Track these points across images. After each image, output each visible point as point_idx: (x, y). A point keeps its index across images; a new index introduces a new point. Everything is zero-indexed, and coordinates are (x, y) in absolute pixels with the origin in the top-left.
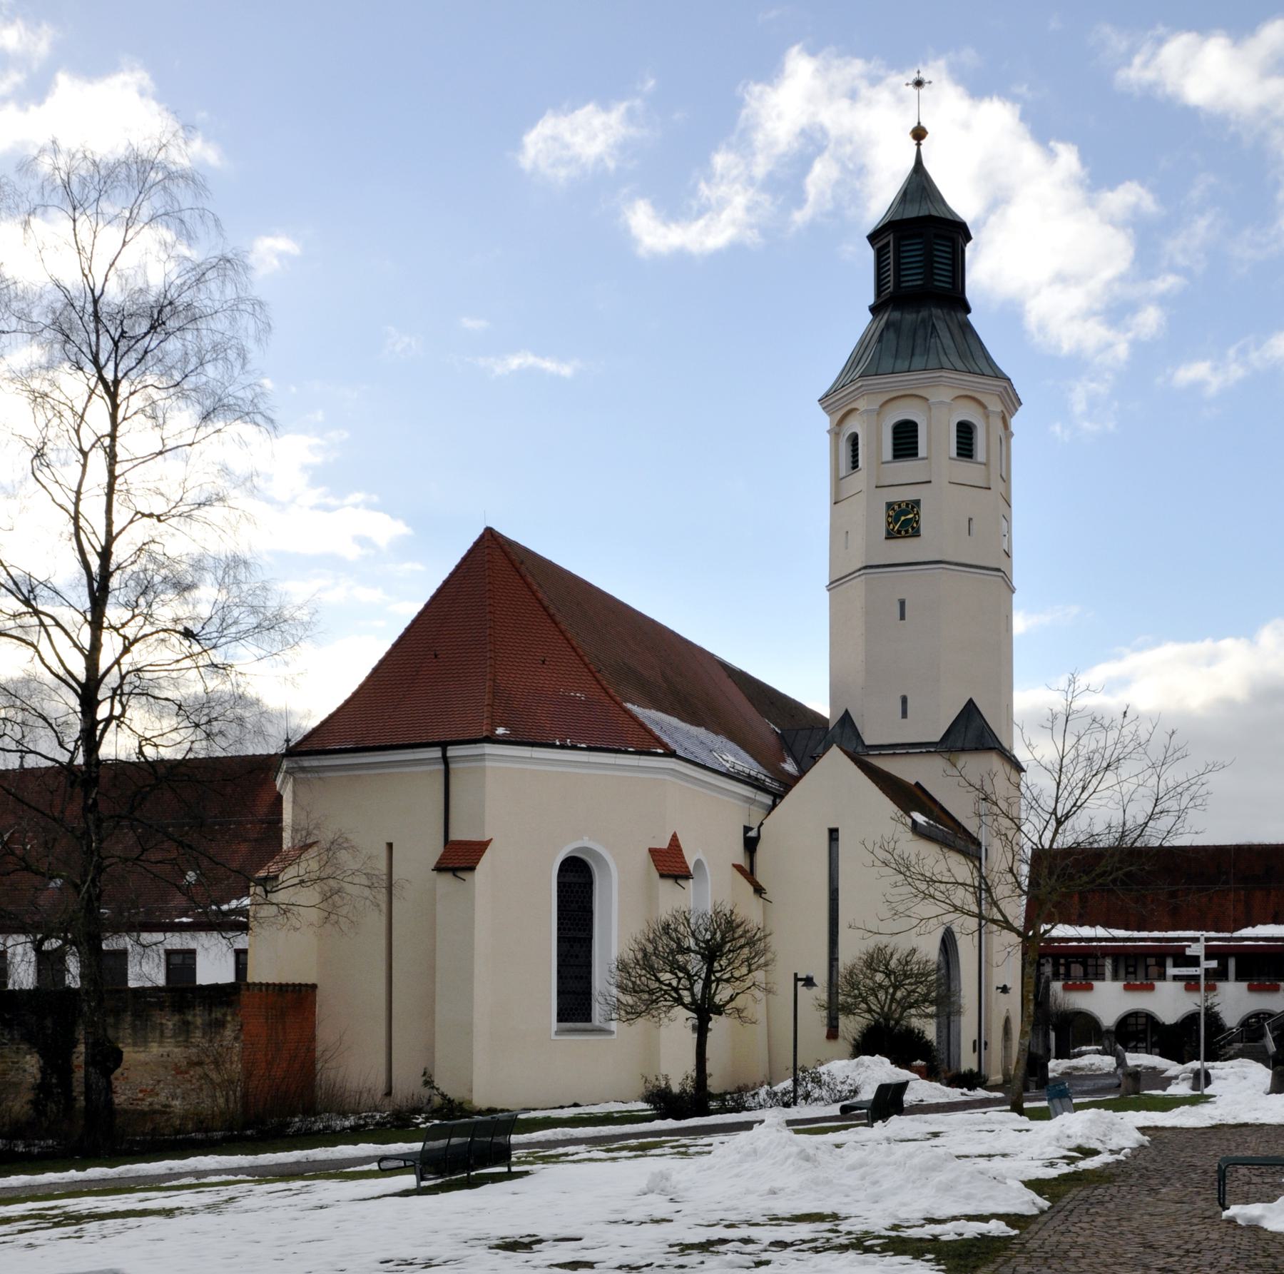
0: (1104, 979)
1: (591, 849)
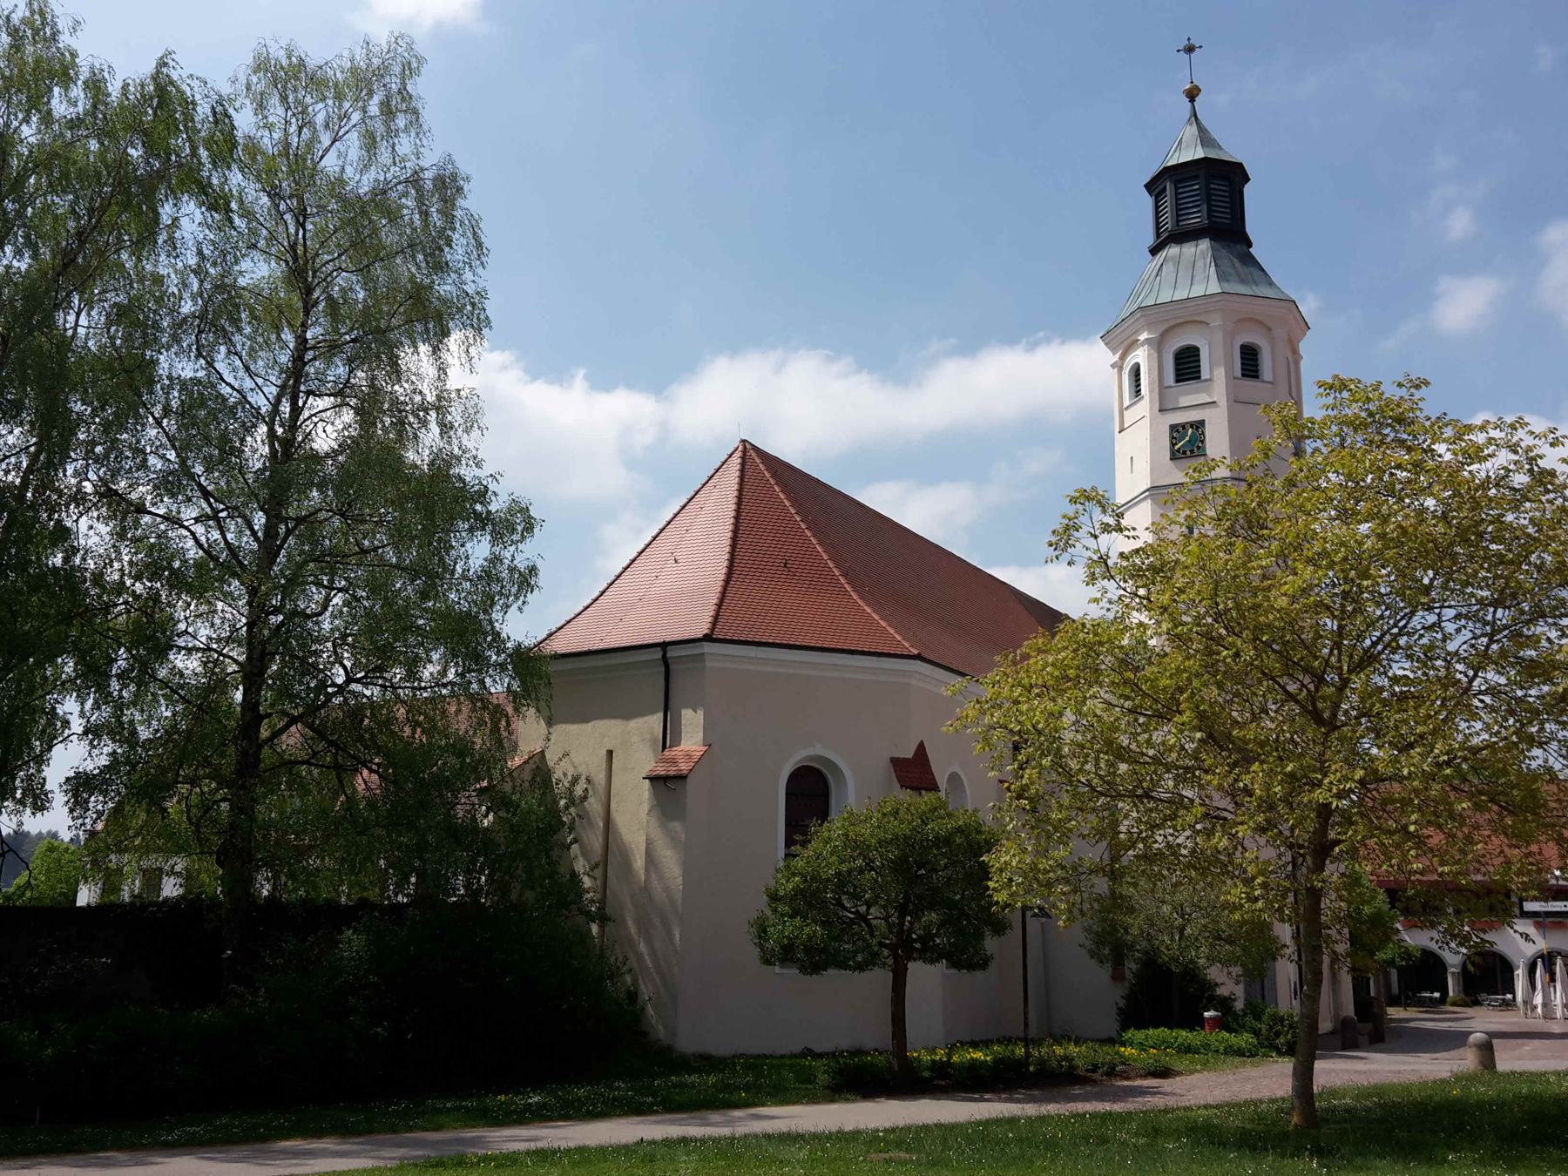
1: (834, 764)
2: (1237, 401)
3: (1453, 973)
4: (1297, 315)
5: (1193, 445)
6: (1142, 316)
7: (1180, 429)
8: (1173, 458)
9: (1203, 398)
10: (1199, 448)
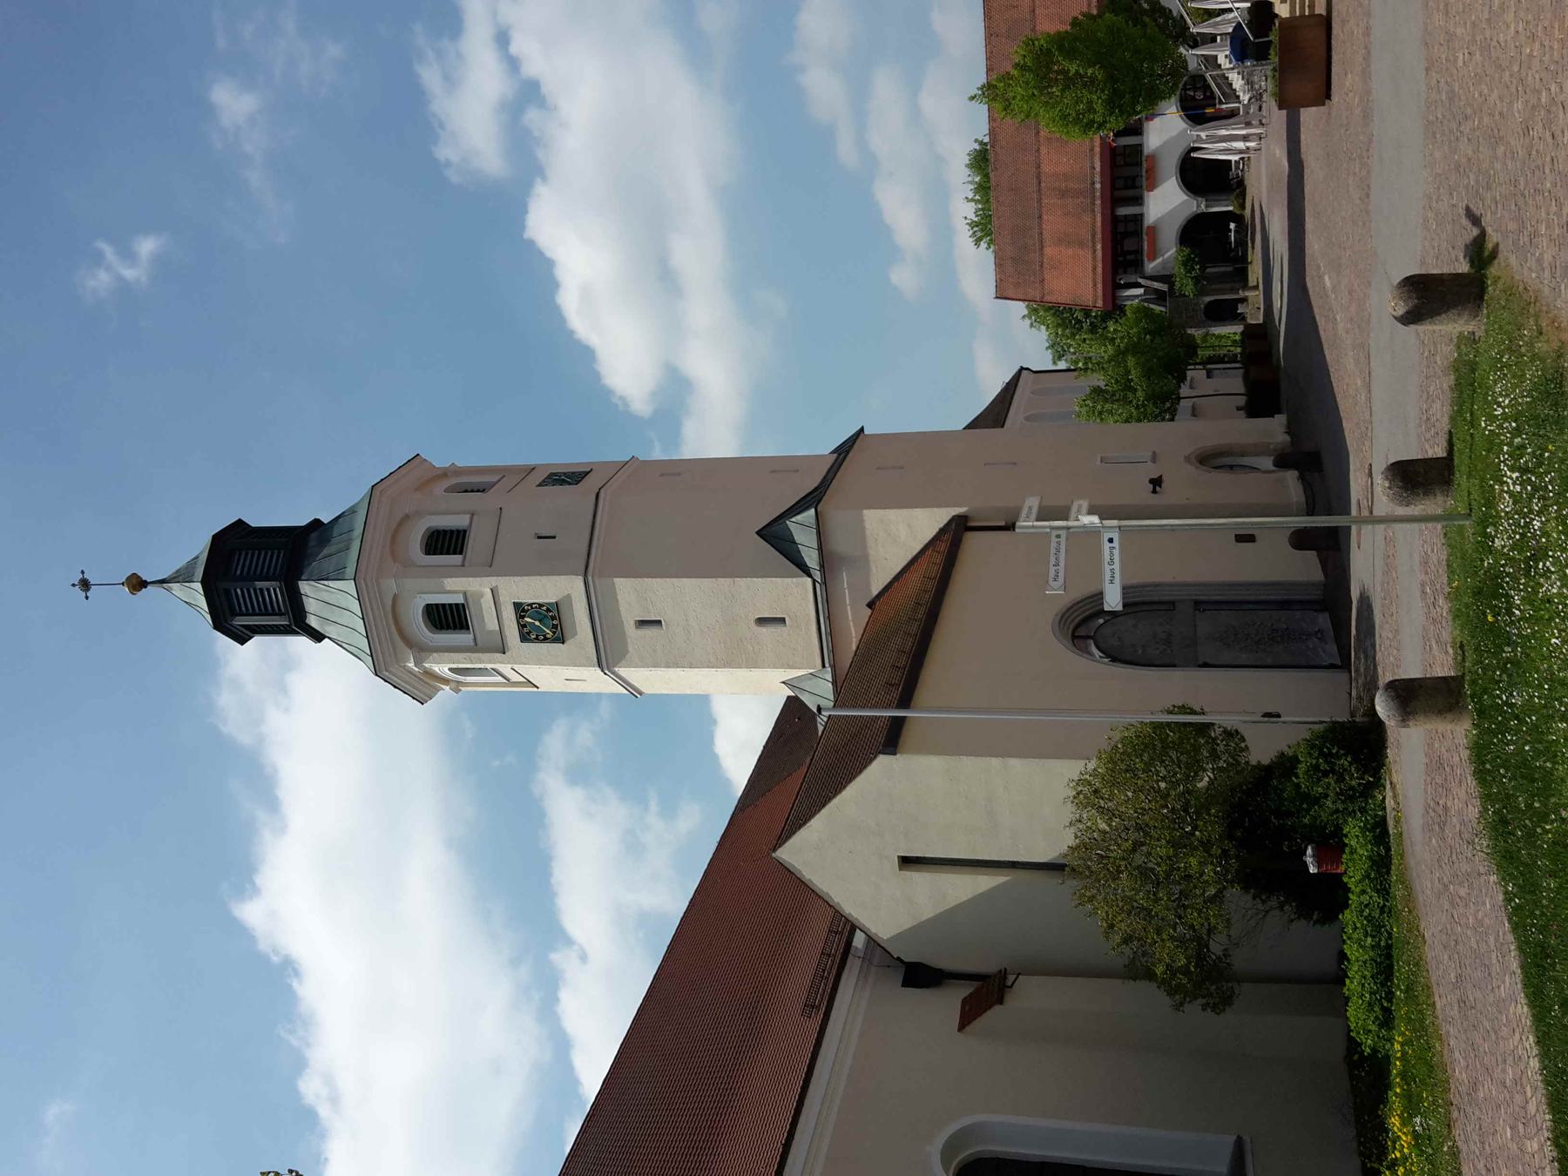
0: (1142, 215)
2: (490, 566)
3: (1207, 206)
4: (402, 471)
5: (546, 616)
6: (387, 671)
8: (561, 640)
10: (548, 610)
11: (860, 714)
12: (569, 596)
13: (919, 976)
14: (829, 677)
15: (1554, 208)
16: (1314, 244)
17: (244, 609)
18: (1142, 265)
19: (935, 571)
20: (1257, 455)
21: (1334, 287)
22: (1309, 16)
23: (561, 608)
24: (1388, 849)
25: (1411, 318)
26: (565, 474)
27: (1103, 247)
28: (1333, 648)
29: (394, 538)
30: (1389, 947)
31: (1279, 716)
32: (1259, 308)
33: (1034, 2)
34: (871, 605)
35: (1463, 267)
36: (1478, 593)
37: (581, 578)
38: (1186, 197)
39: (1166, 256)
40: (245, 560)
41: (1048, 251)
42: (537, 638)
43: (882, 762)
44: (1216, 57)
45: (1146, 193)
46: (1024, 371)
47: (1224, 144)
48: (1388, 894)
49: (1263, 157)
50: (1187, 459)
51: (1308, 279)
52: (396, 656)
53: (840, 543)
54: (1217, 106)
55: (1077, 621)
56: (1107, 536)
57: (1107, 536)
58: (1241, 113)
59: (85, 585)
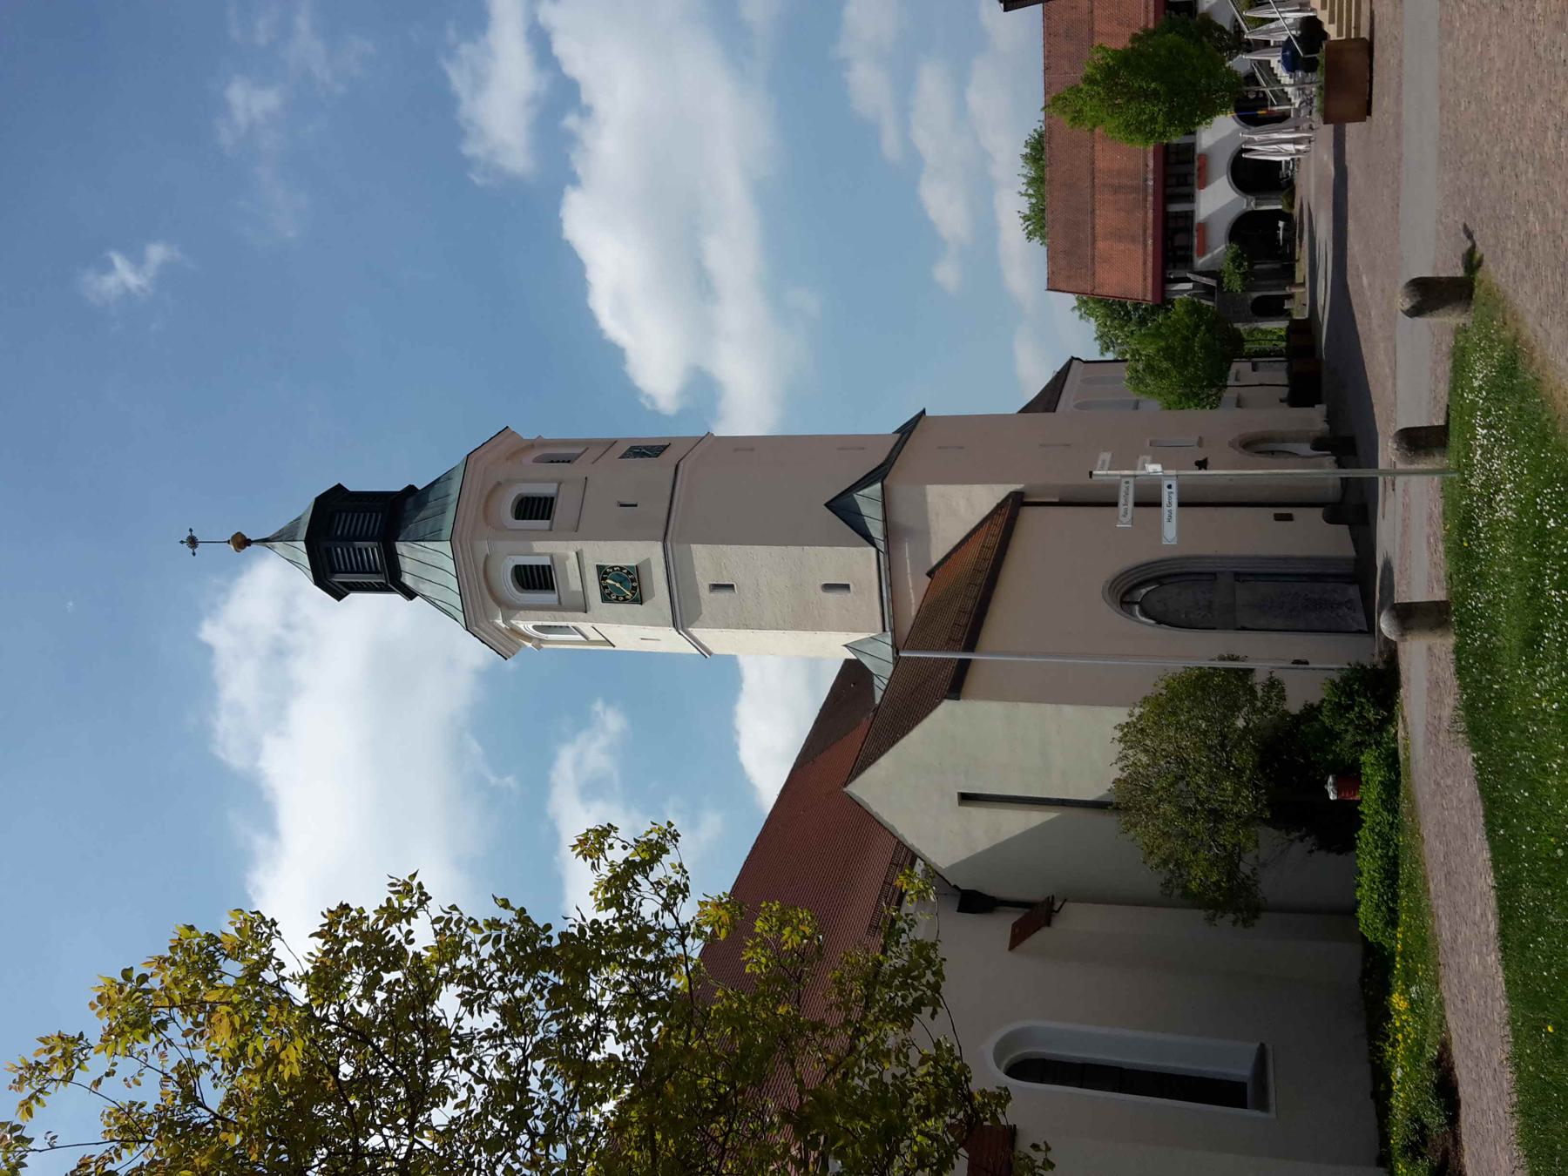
0: (1193, 212)
2: (576, 531)
3: (1256, 205)
4: (486, 448)
5: (626, 579)
6: (477, 626)
7: (606, 591)
9: (572, 562)
10: (629, 573)
11: (936, 656)
12: (648, 559)
13: (973, 902)
14: (889, 641)
15: (1516, 231)
16: (1354, 246)
17: (343, 567)
18: (1192, 261)
19: (993, 541)
20: (1296, 441)
21: (1370, 285)
22: (1354, 39)
23: (641, 571)
24: (1398, 775)
25: (1415, 312)
26: (645, 448)
27: (1154, 243)
28: (1361, 617)
29: (487, 502)
30: (1396, 857)
31: (1307, 663)
32: (1305, 305)
33: (1092, 2)
34: (930, 574)
35: (1460, 272)
36: (1462, 525)
37: (660, 544)
38: (1237, 195)
39: (1216, 252)
40: (352, 520)
41: (1100, 245)
42: (617, 599)
43: (947, 707)
44: (1269, 62)
45: (1197, 190)
46: (1075, 362)
47: (1275, 147)
48: (1396, 812)
49: (1312, 162)
50: (1231, 445)
51: (1348, 278)
52: (486, 613)
53: (903, 514)
54: (1269, 108)
55: (1123, 591)
56: (1166, 483)
57: (1166, 483)
58: (1292, 115)
59: (193, 542)
